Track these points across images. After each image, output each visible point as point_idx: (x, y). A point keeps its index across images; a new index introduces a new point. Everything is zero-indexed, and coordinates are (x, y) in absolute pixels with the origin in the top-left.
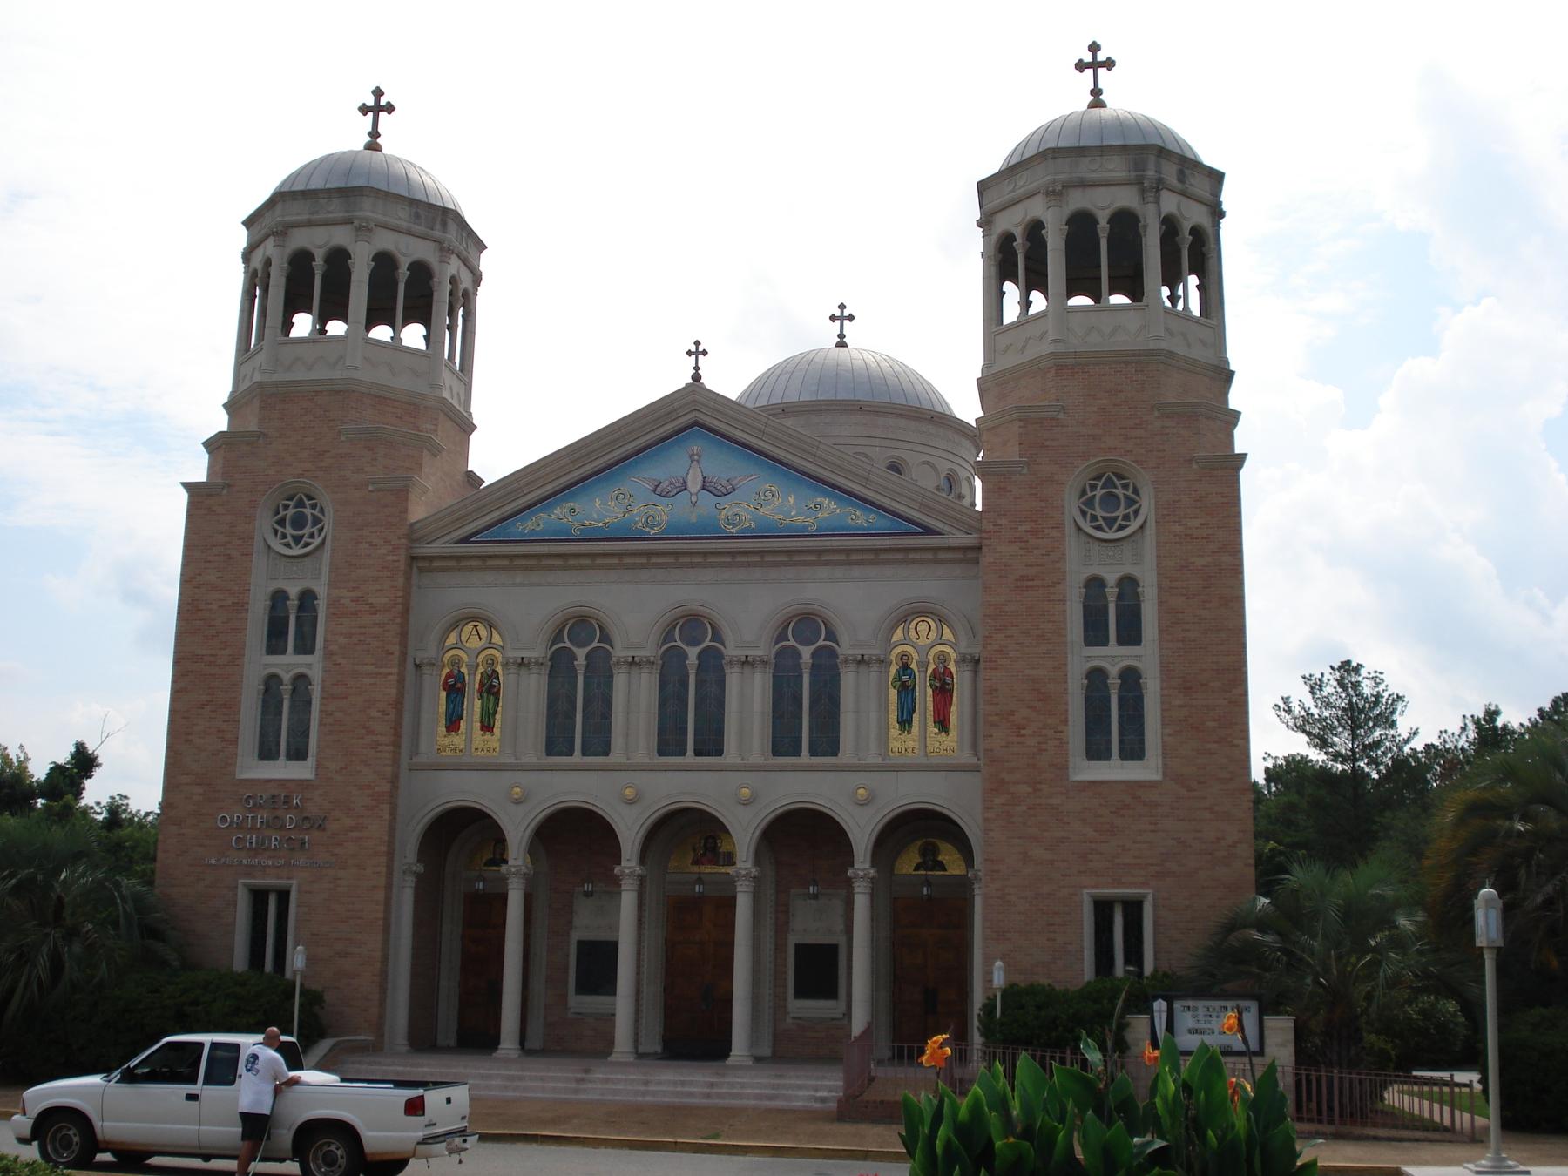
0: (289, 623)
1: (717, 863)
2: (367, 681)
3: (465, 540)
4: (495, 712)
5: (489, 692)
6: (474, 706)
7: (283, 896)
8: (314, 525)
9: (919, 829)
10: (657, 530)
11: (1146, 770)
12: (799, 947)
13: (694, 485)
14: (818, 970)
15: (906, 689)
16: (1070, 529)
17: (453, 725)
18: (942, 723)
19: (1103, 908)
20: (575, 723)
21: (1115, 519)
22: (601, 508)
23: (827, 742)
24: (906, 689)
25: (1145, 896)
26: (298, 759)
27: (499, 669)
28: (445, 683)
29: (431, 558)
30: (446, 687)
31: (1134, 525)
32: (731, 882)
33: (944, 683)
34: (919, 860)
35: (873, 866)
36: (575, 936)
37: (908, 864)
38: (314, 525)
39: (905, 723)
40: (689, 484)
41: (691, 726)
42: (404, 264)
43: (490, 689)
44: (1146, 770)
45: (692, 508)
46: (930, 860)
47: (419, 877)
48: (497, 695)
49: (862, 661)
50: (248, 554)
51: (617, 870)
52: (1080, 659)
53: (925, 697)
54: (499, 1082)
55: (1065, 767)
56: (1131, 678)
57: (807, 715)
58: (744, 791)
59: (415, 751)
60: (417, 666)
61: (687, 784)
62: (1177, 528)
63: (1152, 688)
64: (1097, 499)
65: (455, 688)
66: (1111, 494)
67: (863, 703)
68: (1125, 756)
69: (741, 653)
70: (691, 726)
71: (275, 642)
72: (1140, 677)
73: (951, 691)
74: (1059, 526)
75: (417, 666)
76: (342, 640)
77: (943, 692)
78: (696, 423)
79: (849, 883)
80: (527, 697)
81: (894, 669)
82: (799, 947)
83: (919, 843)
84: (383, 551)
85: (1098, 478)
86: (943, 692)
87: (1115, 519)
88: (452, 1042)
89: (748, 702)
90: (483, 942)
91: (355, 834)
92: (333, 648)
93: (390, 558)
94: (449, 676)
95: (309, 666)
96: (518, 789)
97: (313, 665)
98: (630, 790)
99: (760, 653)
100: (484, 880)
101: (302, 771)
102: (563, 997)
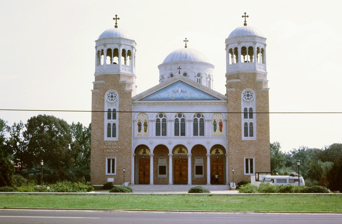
0: (112, 114)
1: (182, 153)
2: (127, 124)
3: (141, 100)
4: (147, 129)
5: (145, 125)
6: (143, 127)
7: (113, 160)
8: (109, 96)
9: (217, 147)
10: (174, 99)
11: (116, 139)
12: (196, 167)
13: (180, 91)
14: (163, 170)
15: (215, 125)
16: (242, 100)
17: (140, 130)
18: (221, 130)
19: (247, 160)
20: (161, 129)
21: (115, 96)
22: (163, 95)
23: (202, 134)
24: (215, 125)
25: (115, 158)
26: (194, 134)
27: (147, 122)
28: (138, 124)
29: (135, 103)
30: (138, 124)
31: (116, 100)
32: (187, 156)
33: (221, 124)
34: (215, 152)
35: (153, 153)
36: (159, 165)
37: (176, 152)
38: (109, 96)
39: (215, 130)
40: (179, 91)
41: (180, 130)
42: (247, 48)
43: (146, 125)
44: (254, 138)
45: (179, 95)
46: (217, 152)
47: (154, 156)
48: (147, 126)
49: (208, 121)
50: (104, 102)
51: (169, 154)
52: (243, 121)
53: (218, 126)
54: (155, 188)
55: (241, 138)
56: (251, 124)
57: (199, 129)
58: (190, 141)
59: (134, 136)
60: (133, 121)
61: (179, 140)
62: (259, 100)
63: (255, 125)
64: (250, 96)
65: (140, 125)
66: (248, 94)
67: (208, 127)
68: (250, 136)
69: (207, 119)
70: (180, 130)
71: (109, 118)
72: (116, 124)
73: (222, 125)
74: (240, 99)
75: (133, 121)
76: (121, 117)
77: (221, 126)
78: (180, 81)
79: (169, 156)
80: (152, 127)
81: (213, 122)
82: (196, 167)
83: (215, 149)
84: (128, 102)
85: (110, 93)
86: (221, 126)
87: (115, 96)
88: (138, 183)
89: (189, 127)
90: (148, 166)
91: (125, 149)
92: (120, 118)
93: (129, 103)
94: (138, 123)
95: (115, 121)
96: (152, 141)
97: (116, 121)
98: (171, 141)
99: (210, 119)
100: (181, 156)
101: (116, 139)
102: (157, 175)
